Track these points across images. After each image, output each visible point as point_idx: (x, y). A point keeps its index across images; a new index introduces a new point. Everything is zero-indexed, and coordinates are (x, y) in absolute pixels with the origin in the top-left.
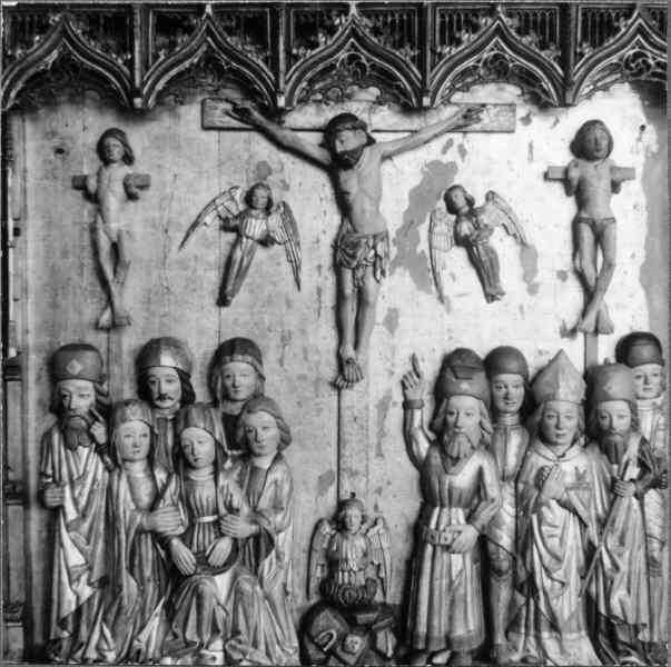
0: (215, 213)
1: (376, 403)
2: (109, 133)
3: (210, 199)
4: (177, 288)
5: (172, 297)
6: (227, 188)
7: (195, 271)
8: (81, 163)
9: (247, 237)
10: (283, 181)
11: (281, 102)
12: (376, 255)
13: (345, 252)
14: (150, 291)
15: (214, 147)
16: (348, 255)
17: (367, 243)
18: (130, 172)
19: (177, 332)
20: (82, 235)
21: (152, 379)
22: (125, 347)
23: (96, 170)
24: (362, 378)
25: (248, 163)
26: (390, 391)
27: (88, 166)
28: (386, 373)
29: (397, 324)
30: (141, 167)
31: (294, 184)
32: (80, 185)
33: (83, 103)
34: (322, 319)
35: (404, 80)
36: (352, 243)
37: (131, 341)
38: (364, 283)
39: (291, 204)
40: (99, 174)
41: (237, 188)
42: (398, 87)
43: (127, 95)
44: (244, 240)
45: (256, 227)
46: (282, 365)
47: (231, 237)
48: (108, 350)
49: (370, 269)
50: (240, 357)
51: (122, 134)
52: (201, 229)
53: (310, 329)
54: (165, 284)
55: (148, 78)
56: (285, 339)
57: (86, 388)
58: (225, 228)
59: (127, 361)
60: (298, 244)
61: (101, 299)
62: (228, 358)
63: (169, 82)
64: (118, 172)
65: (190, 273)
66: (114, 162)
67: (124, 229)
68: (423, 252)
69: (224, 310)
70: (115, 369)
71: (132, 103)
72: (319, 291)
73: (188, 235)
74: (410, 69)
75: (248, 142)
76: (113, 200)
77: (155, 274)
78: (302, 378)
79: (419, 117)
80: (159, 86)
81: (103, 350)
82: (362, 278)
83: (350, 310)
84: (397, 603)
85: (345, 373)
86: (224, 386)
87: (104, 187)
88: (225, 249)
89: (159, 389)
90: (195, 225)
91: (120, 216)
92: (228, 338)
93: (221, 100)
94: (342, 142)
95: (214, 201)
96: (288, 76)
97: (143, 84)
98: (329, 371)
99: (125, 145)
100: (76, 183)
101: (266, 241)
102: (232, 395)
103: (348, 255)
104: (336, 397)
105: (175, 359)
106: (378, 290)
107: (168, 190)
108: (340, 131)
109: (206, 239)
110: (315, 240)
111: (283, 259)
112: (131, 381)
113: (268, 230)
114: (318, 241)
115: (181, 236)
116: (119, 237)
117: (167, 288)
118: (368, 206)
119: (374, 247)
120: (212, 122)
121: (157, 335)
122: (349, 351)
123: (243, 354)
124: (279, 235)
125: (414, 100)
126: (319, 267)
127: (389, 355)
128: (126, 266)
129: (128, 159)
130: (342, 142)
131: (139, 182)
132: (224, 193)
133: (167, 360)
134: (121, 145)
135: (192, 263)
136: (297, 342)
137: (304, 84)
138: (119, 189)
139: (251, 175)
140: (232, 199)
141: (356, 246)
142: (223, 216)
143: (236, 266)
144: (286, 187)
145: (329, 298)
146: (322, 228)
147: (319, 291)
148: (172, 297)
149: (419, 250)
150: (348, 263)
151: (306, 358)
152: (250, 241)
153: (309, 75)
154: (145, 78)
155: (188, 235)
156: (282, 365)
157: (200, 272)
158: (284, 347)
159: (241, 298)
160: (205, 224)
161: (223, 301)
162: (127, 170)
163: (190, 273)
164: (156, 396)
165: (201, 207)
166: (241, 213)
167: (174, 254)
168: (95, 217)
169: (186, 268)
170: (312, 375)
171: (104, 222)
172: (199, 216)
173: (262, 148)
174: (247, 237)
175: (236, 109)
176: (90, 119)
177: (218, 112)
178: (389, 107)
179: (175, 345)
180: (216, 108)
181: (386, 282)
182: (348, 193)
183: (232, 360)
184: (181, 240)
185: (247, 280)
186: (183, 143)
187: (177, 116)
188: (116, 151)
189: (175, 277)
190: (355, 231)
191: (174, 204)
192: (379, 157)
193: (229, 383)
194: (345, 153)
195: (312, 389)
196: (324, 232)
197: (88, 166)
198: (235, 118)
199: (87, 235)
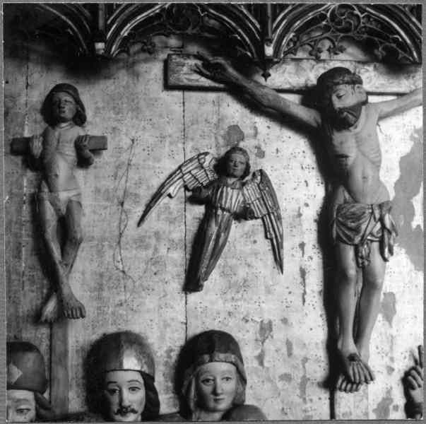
0: (180, 182)
1: (375, 407)
2: (58, 88)
3: (175, 167)
4: (136, 270)
5: (129, 283)
6: (194, 154)
7: (156, 250)
8: (22, 126)
9: (223, 209)
10: (258, 148)
11: (269, 51)
12: (383, 227)
13: (335, 231)
14: (101, 275)
15: (178, 109)
16: (351, 229)
17: (372, 213)
18: (82, 134)
19: (136, 326)
20: (19, 211)
21: (111, 387)
22: (71, 342)
23: (39, 131)
24: (372, 379)
25: (217, 126)
26: (389, 392)
27: (31, 128)
28: (385, 372)
29: (394, 312)
30: (94, 127)
31: (269, 150)
32: (20, 148)
33: (28, 59)
34: (308, 308)
35: (402, 33)
36: (353, 214)
37: (79, 335)
38: (369, 261)
39: (268, 172)
40: (45, 135)
41: (206, 154)
42: (396, 41)
43: (86, 37)
44: (220, 212)
45: (232, 198)
46: (261, 363)
47: (200, 210)
48: (51, 348)
49: (375, 245)
50: (222, 356)
51: (75, 90)
52: (164, 200)
53: (293, 318)
54: (121, 267)
55: (113, 23)
56: (266, 329)
57: (26, 400)
58: (194, 199)
59: (74, 362)
60: (279, 218)
61: (42, 287)
62: (207, 357)
63: (135, 29)
64: (68, 133)
65: (150, 252)
66: (64, 120)
67: (74, 199)
68: (418, 226)
69: (194, 297)
70: (59, 373)
71: (93, 49)
72: (303, 273)
73: (149, 208)
74: (410, 20)
75: (217, 103)
76: (63, 166)
77: (108, 254)
78: (286, 377)
79: (407, 78)
80: (125, 32)
81: (44, 347)
82: (368, 256)
83: (345, 297)
84: (70, 411)
85: (342, 371)
86: (200, 393)
87: (51, 148)
88: (193, 227)
89: (121, 400)
90: (156, 197)
91: (72, 185)
92: (198, 331)
93: (188, 56)
94: (339, 97)
95: (180, 168)
96: (274, 25)
97: (108, 28)
98: (319, 369)
99: (78, 102)
100: (15, 147)
101: (244, 214)
102: (212, 404)
103: (351, 229)
104: (327, 402)
105: (139, 360)
106: (384, 268)
107: (124, 157)
108: (338, 84)
109: (170, 213)
110: (296, 214)
111: (260, 236)
112: (78, 385)
113: (244, 201)
114: (300, 215)
115: (140, 210)
116: (69, 209)
117: (123, 272)
118: (370, 172)
119: (381, 220)
120: (179, 79)
121: (112, 329)
122: (350, 346)
123: (225, 352)
124: (258, 209)
125: (415, 54)
126: (302, 246)
127: (387, 348)
128: (77, 244)
129: (80, 119)
130: (339, 97)
131: (93, 145)
132: (191, 160)
133: (131, 362)
134: (74, 102)
135: (153, 241)
136: (279, 334)
137: (291, 35)
138: (70, 152)
139: (221, 141)
140: (201, 166)
141: (357, 217)
142: (191, 186)
143: (212, 244)
144: (261, 154)
145: (315, 281)
146: (303, 199)
147: (303, 273)
148: (129, 283)
149: (414, 225)
150: (351, 239)
151: (290, 354)
152: (227, 214)
153: (298, 24)
154: (109, 22)
155: (149, 208)
156: (261, 363)
157: (163, 251)
158: (263, 342)
159: (214, 281)
160: (170, 196)
161: (192, 282)
162: (77, 131)
163: (150, 252)
164: (115, 408)
165: (167, 173)
166: (211, 183)
167: (131, 231)
168: (39, 187)
169: (147, 248)
170: (298, 376)
171: (51, 191)
172: (163, 186)
173: (234, 111)
174: (223, 209)
175: (207, 65)
176: (36, 76)
177: (185, 69)
178: (375, 68)
179: (135, 341)
180: (183, 65)
181: (392, 260)
182: (347, 157)
183: (211, 361)
184: (140, 214)
185: (220, 262)
186: (142, 104)
187: (136, 75)
188: (68, 111)
189: (135, 260)
190: (356, 201)
191: (132, 174)
192: (377, 116)
193: (207, 389)
194: (341, 110)
195: (298, 392)
196: (307, 205)
197: (31, 128)
198: (207, 77)
199: (26, 209)
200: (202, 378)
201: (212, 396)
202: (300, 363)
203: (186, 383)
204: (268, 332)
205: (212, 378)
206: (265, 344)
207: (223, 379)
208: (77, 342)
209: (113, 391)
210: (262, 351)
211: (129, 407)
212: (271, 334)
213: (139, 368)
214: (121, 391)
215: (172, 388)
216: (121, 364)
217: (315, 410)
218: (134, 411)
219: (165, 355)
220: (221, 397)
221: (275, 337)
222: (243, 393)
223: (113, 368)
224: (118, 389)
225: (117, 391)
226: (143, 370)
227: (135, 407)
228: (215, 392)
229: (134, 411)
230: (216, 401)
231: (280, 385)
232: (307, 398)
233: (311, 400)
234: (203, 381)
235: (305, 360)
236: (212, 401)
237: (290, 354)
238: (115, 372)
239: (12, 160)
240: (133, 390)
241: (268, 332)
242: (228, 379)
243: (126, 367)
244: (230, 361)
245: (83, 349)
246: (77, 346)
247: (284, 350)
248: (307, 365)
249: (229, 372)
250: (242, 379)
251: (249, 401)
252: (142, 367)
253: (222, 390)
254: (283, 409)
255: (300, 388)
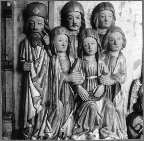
21: (70, 17)
46: (120, 15)
62: (103, 8)
78: (129, 21)
86: (100, 22)
89: (74, 21)
102: (104, 25)
151: (131, 13)
156: (120, 15)
164: (71, 24)
170: (133, 20)
183: (105, 10)
193: (103, 20)
200: (101, 16)
201: (104, 22)
202: (134, 16)
203: (95, 18)
204: (123, 5)
205: (105, 16)
206: (122, 9)
207: (108, 16)
208: (57, 5)
209: (71, 18)
210: (121, 11)
211: (76, 24)
212: (125, 6)
213: (80, 11)
214: (73, 19)
215: (89, 22)
216: (74, 9)
217: (138, 32)
218: (77, 26)
219: (88, 11)
220: (92, 50)
221: (126, 7)
222: (114, 23)
223: (71, 10)
224: (73, 18)
225: (72, 18)
226: (81, 12)
227: (78, 24)
228: (106, 21)
229: (77, 26)
230: (90, 51)
231: (127, 23)
232: (136, 28)
233: (137, 29)
234: (101, 17)
235: (136, 15)
236: (104, 24)
237: (131, 13)
238: (71, 12)
239: (20, 15)
240: (78, 18)
241: (123, 5)
242: (110, 16)
243: (75, 10)
244: (111, 10)
245: (59, 8)
246: (57, 7)
247: (129, 11)
248: (136, 17)
249: (110, 14)
250: (115, 18)
251: (116, 25)
252: (81, 11)
253: (92, 47)
254: (127, 31)
255: (133, 25)
